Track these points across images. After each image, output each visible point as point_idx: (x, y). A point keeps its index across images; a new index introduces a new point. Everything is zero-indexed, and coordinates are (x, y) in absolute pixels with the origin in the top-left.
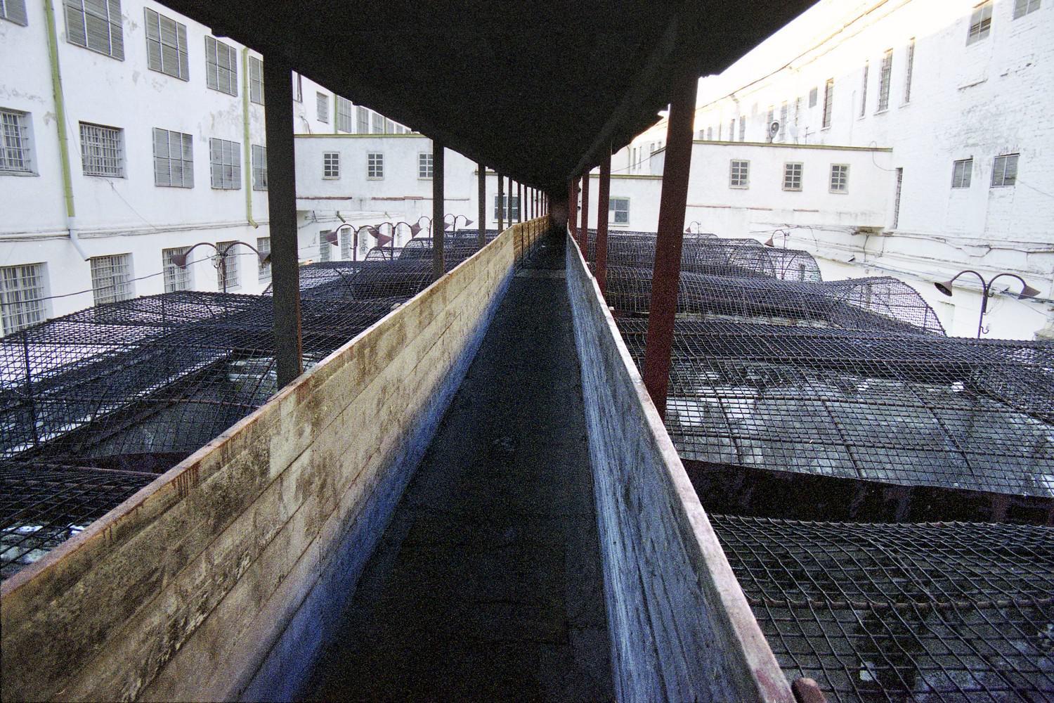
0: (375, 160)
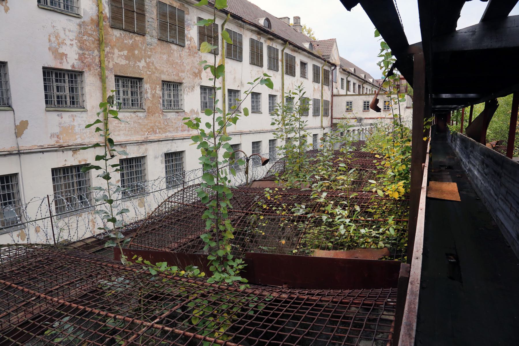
0: (366, 104)
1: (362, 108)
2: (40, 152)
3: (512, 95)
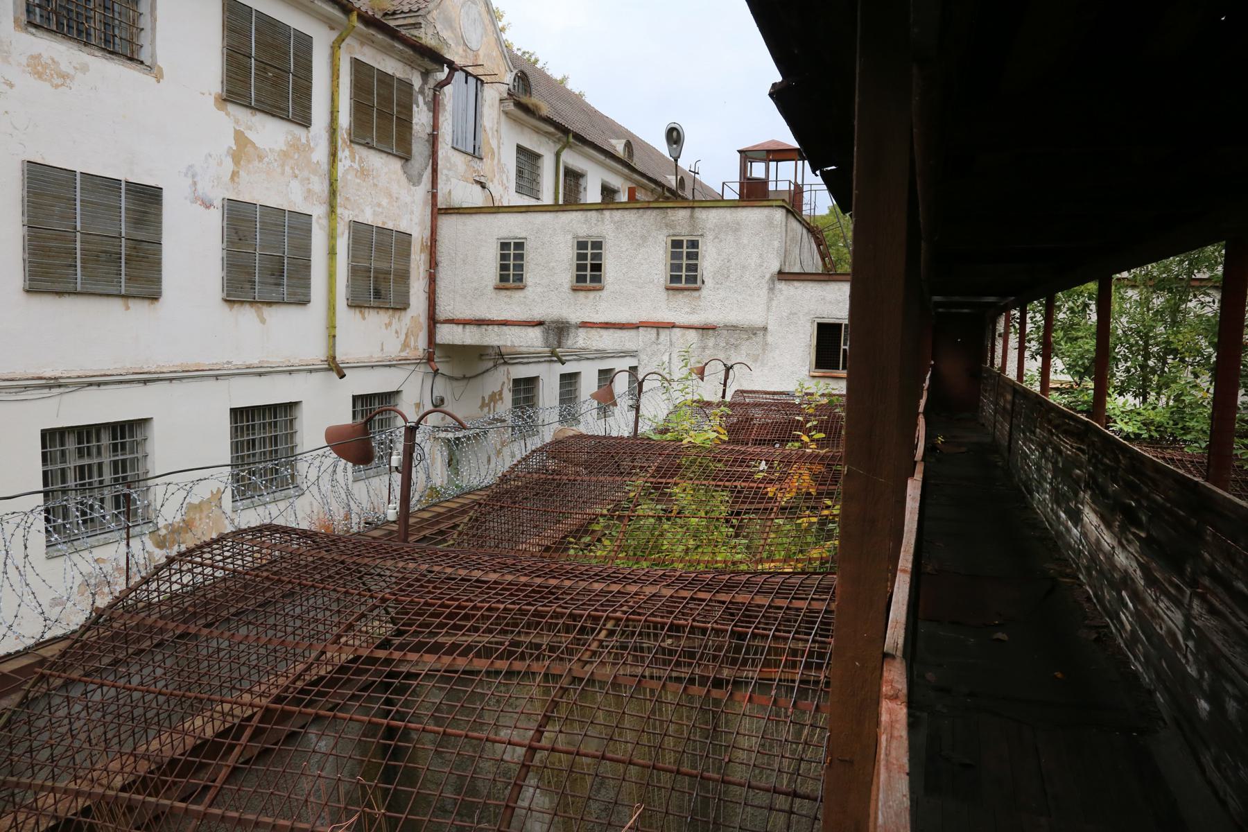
0: (589, 251)
1: (566, 276)
2: (139, 381)
3: (1224, 242)
